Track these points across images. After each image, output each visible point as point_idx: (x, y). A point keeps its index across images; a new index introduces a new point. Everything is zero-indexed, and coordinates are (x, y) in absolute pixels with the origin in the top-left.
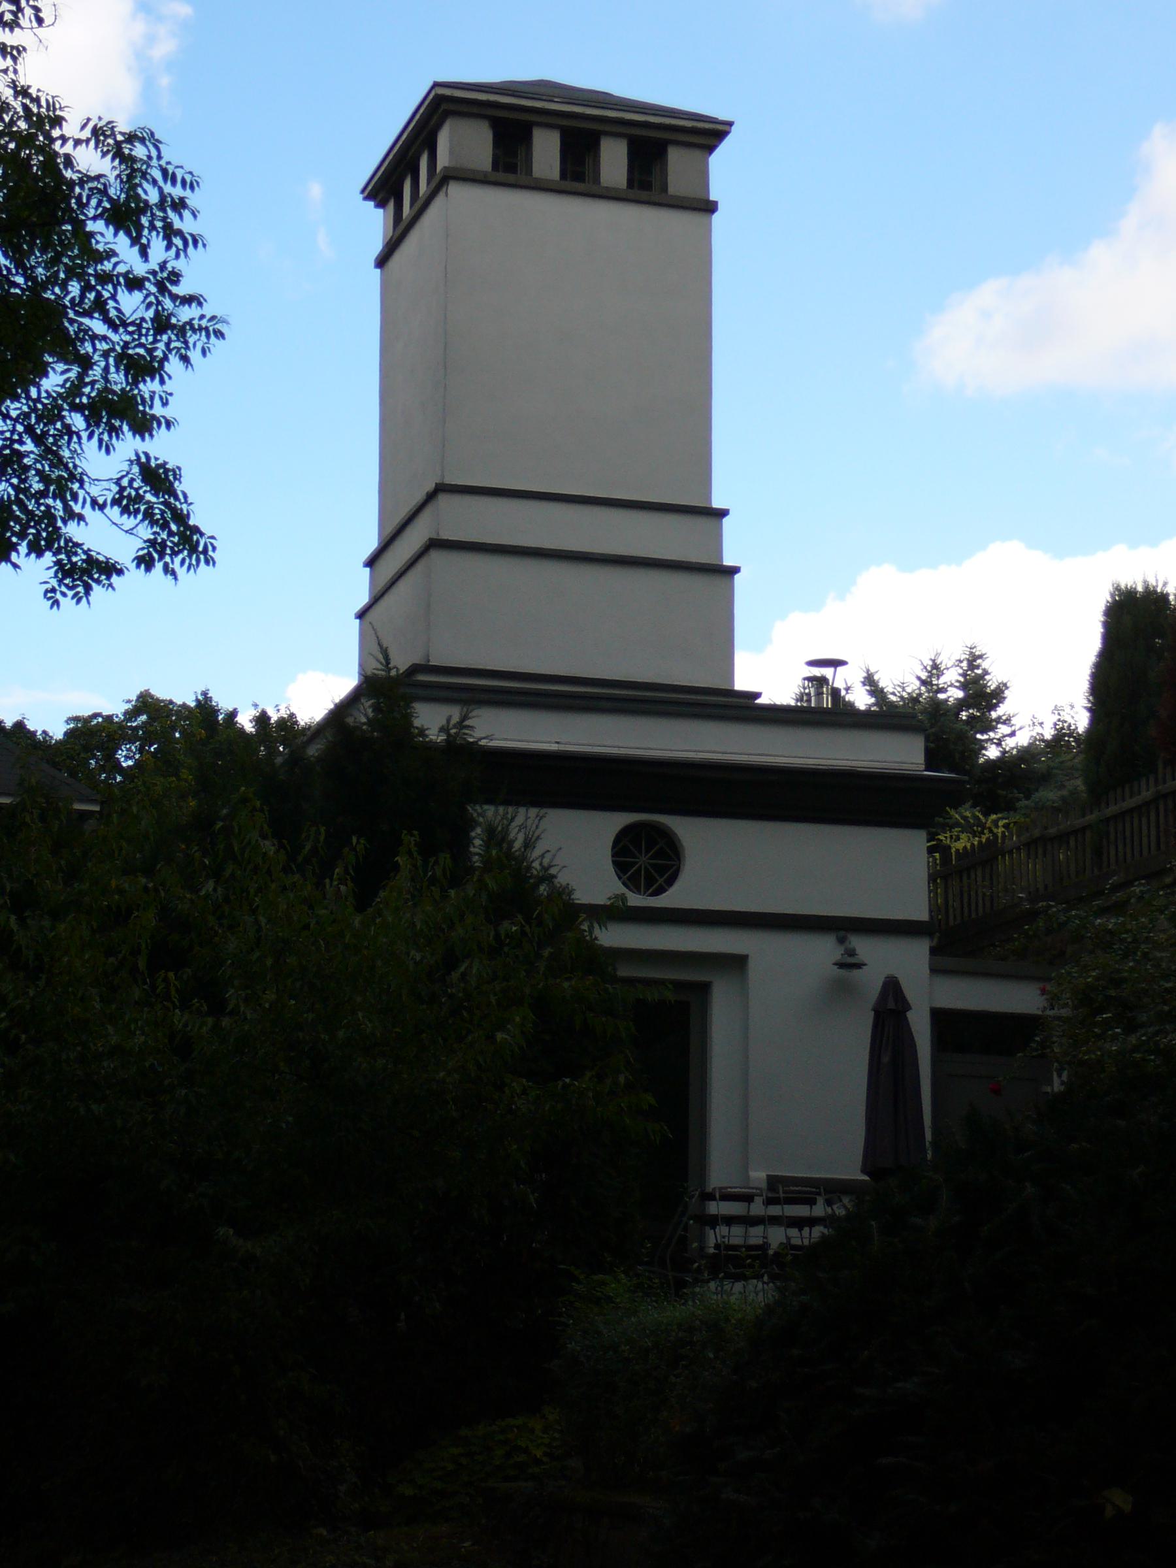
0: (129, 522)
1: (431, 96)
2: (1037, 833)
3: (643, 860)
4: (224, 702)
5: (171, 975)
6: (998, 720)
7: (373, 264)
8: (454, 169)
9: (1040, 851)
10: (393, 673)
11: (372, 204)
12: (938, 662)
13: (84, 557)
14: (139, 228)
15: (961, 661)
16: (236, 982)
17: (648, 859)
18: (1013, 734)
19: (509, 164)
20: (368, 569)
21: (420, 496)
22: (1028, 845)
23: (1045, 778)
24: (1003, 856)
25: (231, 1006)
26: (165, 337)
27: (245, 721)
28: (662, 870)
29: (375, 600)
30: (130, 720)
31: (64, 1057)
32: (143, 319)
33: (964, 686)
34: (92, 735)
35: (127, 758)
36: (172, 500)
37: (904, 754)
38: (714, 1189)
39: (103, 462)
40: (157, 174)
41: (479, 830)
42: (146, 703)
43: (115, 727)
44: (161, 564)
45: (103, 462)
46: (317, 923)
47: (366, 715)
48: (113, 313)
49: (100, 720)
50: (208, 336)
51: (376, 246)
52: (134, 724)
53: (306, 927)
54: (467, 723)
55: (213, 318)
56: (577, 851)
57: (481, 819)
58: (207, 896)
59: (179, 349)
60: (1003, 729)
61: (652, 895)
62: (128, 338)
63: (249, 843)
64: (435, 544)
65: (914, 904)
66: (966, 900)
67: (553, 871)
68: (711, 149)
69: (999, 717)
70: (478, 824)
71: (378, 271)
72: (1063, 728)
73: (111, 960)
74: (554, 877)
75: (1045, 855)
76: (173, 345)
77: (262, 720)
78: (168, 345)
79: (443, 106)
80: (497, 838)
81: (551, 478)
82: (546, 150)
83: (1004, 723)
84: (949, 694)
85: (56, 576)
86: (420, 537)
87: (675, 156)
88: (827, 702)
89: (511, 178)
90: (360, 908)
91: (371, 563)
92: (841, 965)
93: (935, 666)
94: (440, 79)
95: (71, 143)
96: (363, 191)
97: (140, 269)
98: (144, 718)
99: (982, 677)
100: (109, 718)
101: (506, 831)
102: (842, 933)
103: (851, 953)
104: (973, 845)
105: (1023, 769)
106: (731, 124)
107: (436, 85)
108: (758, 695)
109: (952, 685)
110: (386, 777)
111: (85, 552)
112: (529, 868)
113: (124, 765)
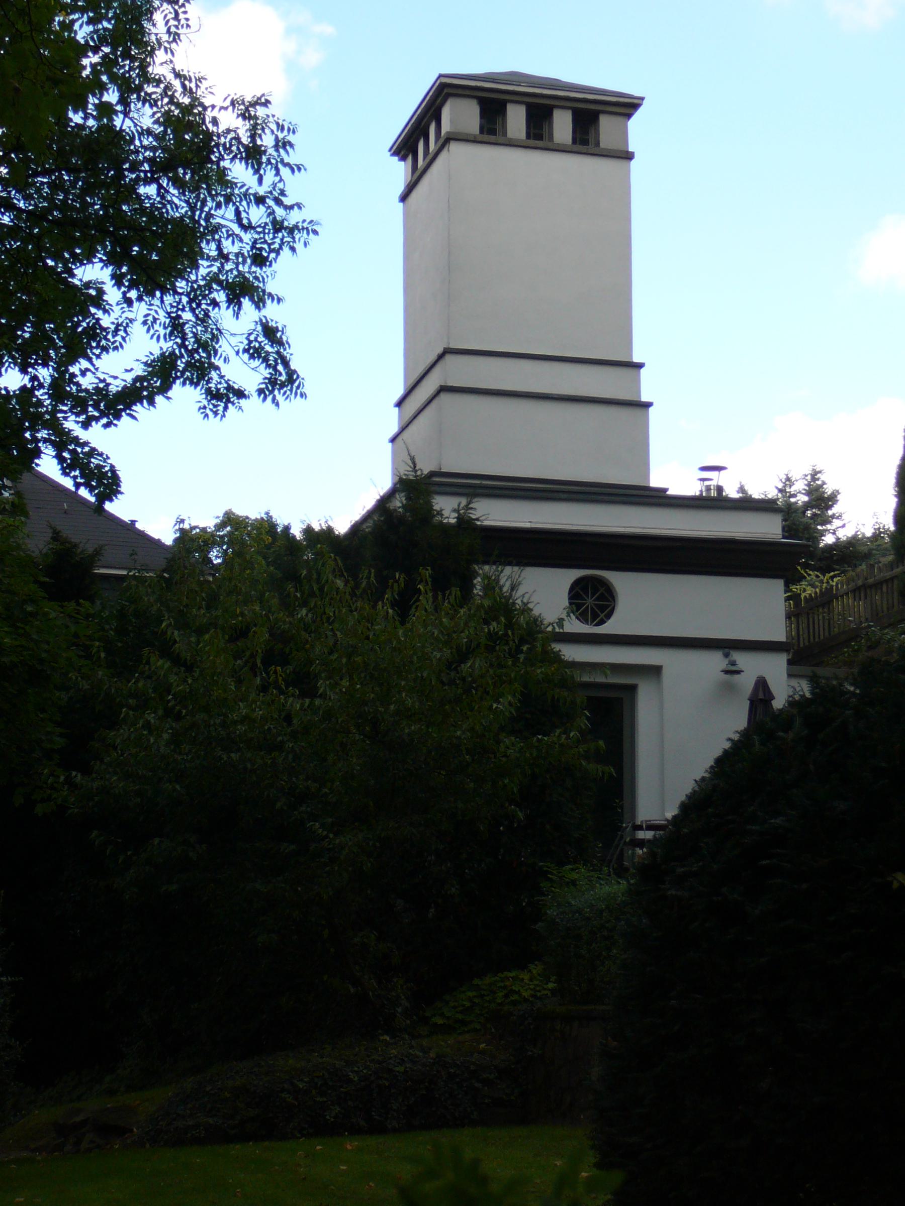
0: (256, 363)
1: (437, 84)
2: (860, 583)
3: (590, 602)
4: (281, 519)
5: (279, 668)
6: (833, 516)
7: (397, 200)
8: (453, 133)
9: (862, 595)
10: (419, 473)
11: (396, 158)
12: (790, 476)
13: (225, 385)
14: (260, 164)
15: (806, 476)
16: (323, 675)
17: (594, 601)
18: (844, 526)
19: (491, 127)
20: (397, 409)
21: (433, 357)
22: (854, 591)
23: (867, 556)
24: (837, 599)
25: (321, 691)
26: (280, 235)
27: (297, 531)
28: (602, 608)
29: (403, 429)
30: (218, 530)
31: (212, 723)
32: (266, 224)
33: (808, 493)
34: (191, 541)
35: (217, 557)
36: (282, 350)
37: (769, 529)
38: (642, 822)
39: (236, 324)
40: (274, 127)
41: (479, 579)
42: (229, 519)
43: (207, 536)
44: (271, 396)
45: (236, 324)
46: (374, 634)
47: (401, 502)
48: (245, 221)
49: (198, 530)
50: (308, 233)
51: (400, 188)
52: (221, 533)
53: (368, 638)
54: (471, 506)
55: (311, 222)
56: (545, 592)
57: (481, 572)
58: (302, 618)
59: (289, 242)
60: (836, 523)
61: (596, 625)
62: (256, 236)
63: (327, 581)
64: (444, 389)
65: (778, 633)
66: (811, 631)
67: (530, 606)
68: (629, 116)
69: (834, 515)
70: (478, 575)
71: (401, 204)
72: (879, 528)
73: (239, 662)
74: (532, 610)
75: (866, 598)
76: (285, 240)
77: (308, 531)
78: (282, 240)
79: (445, 90)
80: (491, 586)
81: (521, 347)
82: (516, 119)
83: (837, 518)
84: (798, 498)
85: (206, 398)
86: (436, 381)
87: (606, 123)
88: (713, 493)
89: (492, 138)
90: (403, 623)
91: (399, 404)
92: (727, 672)
93: (788, 479)
94: (443, 72)
95: (217, 109)
96: (390, 150)
97: (262, 191)
98: (229, 528)
99: (821, 486)
100: (204, 530)
101: (497, 580)
102: (727, 650)
103: (733, 663)
104: (816, 593)
105: (850, 553)
106: (643, 99)
107: (440, 76)
108: (666, 490)
109: (800, 492)
110: (415, 540)
111: (226, 382)
112: (514, 603)
113: (215, 562)
